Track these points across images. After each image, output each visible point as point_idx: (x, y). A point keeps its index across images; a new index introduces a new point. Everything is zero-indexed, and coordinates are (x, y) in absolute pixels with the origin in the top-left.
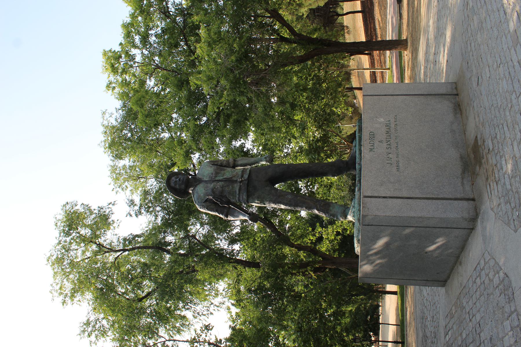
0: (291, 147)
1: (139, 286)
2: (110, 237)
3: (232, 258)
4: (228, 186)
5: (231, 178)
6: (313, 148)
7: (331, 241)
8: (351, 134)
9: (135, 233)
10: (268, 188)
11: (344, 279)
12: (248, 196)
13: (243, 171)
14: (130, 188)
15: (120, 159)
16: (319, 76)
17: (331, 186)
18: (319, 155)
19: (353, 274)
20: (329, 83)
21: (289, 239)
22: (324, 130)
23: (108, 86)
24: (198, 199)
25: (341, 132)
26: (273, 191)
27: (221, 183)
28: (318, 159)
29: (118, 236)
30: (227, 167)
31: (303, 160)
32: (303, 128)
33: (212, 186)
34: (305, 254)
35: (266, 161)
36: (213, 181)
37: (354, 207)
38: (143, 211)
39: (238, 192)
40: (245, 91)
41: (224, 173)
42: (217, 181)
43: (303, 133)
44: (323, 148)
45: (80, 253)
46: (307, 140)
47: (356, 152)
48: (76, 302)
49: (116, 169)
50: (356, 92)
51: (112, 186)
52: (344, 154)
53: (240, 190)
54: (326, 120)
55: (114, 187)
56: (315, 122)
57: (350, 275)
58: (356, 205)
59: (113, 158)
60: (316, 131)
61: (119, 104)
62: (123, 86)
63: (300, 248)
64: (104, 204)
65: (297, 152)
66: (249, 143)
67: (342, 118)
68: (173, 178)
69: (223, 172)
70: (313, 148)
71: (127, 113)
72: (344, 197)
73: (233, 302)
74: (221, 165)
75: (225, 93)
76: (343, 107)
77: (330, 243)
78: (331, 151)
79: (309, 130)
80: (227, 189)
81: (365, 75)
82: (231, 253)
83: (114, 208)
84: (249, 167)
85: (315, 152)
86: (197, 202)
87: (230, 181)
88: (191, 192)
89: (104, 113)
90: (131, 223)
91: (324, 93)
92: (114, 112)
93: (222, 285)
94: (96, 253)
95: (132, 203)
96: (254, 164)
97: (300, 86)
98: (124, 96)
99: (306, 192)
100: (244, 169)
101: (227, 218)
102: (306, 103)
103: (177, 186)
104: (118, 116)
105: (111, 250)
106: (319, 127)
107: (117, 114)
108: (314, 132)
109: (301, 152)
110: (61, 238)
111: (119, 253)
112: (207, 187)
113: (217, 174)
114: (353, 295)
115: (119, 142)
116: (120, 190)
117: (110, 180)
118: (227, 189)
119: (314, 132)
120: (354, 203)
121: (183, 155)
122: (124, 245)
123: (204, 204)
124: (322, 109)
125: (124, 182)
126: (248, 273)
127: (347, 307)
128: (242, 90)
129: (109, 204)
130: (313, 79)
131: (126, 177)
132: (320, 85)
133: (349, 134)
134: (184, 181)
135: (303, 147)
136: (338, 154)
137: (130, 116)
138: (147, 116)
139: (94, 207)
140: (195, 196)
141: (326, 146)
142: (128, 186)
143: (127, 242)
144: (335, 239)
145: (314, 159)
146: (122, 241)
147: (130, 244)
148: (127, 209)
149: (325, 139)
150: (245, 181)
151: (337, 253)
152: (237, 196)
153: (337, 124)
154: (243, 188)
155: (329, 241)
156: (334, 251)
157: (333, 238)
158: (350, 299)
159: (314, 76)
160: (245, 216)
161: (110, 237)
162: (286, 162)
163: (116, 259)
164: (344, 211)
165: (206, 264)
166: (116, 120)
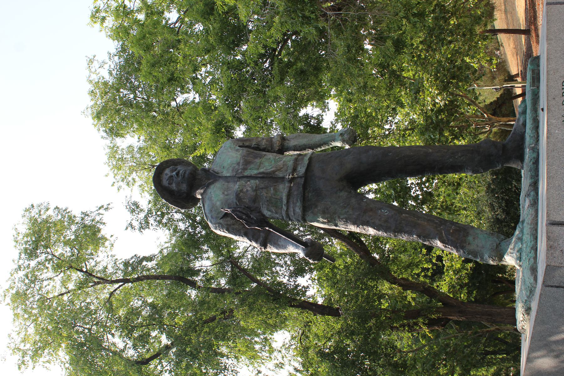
0: (396, 121)
1: (144, 339)
2: (102, 260)
3: (295, 300)
4: (266, 188)
5: (274, 172)
6: (432, 123)
7: (456, 272)
8: (491, 103)
9: (142, 254)
10: (343, 194)
11: (476, 333)
12: (305, 210)
13: (297, 159)
14: (139, 182)
15: (117, 136)
16: (443, 6)
17: (459, 185)
18: (441, 134)
19: (491, 325)
20: (461, 17)
21: (389, 271)
22: (452, 94)
23: (93, 16)
24: (211, 211)
25: (476, 98)
26: (353, 201)
27: (253, 182)
28: (439, 141)
29: (115, 258)
30: (268, 151)
31: (415, 141)
32: (417, 90)
33: (236, 187)
34: (414, 296)
35: (343, 141)
36: (240, 178)
37: (520, 239)
38: (151, 221)
39: (285, 201)
40: (313, 16)
41: (261, 163)
42: (247, 177)
43: (416, 98)
44: (448, 122)
45: (54, 284)
46: (422, 110)
47: (524, 125)
48: (42, 363)
49: (116, 152)
50: (501, 37)
51: (111, 179)
52: (481, 134)
53: (289, 196)
54: (453, 76)
55: (114, 181)
56: (435, 80)
57: (486, 327)
58: (527, 237)
59: (105, 135)
60: (437, 94)
61: (113, 46)
62: (117, 16)
63: (406, 285)
64: (91, 207)
65: (406, 129)
66: (329, 114)
67: (478, 75)
68: (167, 171)
69: (258, 161)
70: (432, 123)
71: (126, 61)
72: (478, 200)
73: (297, 365)
74: (258, 148)
75: (277, 19)
76: (483, 58)
77: (455, 274)
78: (461, 129)
79: (427, 93)
80: (264, 193)
81: (517, 9)
82: (293, 289)
83: (107, 217)
84: (310, 151)
85: (435, 128)
86: (209, 215)
87: (271, 178)
88: (199, 197)
89: (91, 61)
90: (137, 238)
91: (452, 33)
92: (107, 60)
93: (281, 338)
94: (81, 285)
95: (134, 208)
96: (320, 146)
97: (412, 8)
98: (120, 33)
99: (419, 193)
100: (300, 155)
101: (265, 248)
102: (421, 51)
103: (174, 187)
104: (112, 67)
105: (104, 280)
106: (444, 88)
107: (110, 63)
108: (434, 98)
109: (412, 129)
110: (21, 262)
111: (116, 286)
112: (228, 189)
113: (247, 163)
114: (488, 353)
115: (116, 108)
116: (123, 185)
117: (107, 169)
118: (264, 193)
119: (434, 98)
120: (522, 231)
121: (212, 130)
122: (125, 273)
123: (221, 221)
124: (447, 59)
125: (131, 173)
126: (320, 324)
127: (477, 371)
128: (307, 14)
129: (100, 208)
130: (433, 11)
131: (134, 164)
132: (446, 20)
133: (488, 102)
134: (186, 176)
135: (415, 122)
136: (470, 133)
137: (129, 68)
138: (153, 65)
139: (77, 212)
140: (206, 206)
141: (454, 120)
142: (137, 179)
143: (130, 268)
144: (463, 268)
145: (433, 140)
146: (121, 266)
147: (134, 272)
148: (128, 217)
149: (451, 108)
150: (299, 180)
151: (465, 290)
152: (285, 208)
153: (470, 86)
154: (295, 193)
155: (454, 271)
156: (462, 287)
157: (458, 266)
158: (483, 359)
159: (435, 6)
160: (297, 247)
161: (102, 260)
162: (388, 143)
163: (112, 294)
164: (498, 245)
165: (251, 309)
166: (111, 73)
